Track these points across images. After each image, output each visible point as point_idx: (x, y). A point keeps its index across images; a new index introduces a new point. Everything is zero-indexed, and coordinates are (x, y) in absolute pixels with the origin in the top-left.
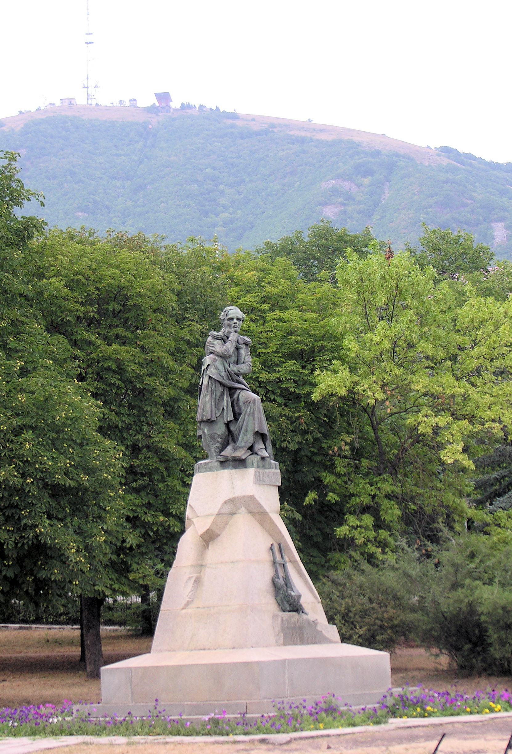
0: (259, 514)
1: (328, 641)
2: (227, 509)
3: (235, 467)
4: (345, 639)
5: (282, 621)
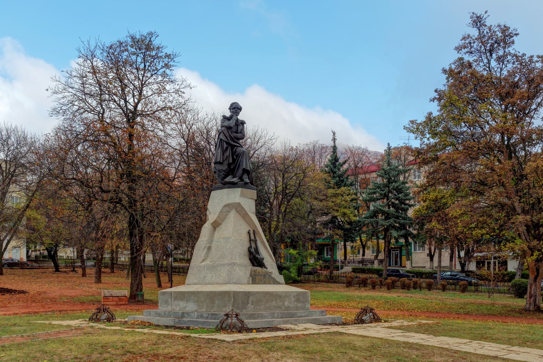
1: (279, 283)
4: (287, 283)
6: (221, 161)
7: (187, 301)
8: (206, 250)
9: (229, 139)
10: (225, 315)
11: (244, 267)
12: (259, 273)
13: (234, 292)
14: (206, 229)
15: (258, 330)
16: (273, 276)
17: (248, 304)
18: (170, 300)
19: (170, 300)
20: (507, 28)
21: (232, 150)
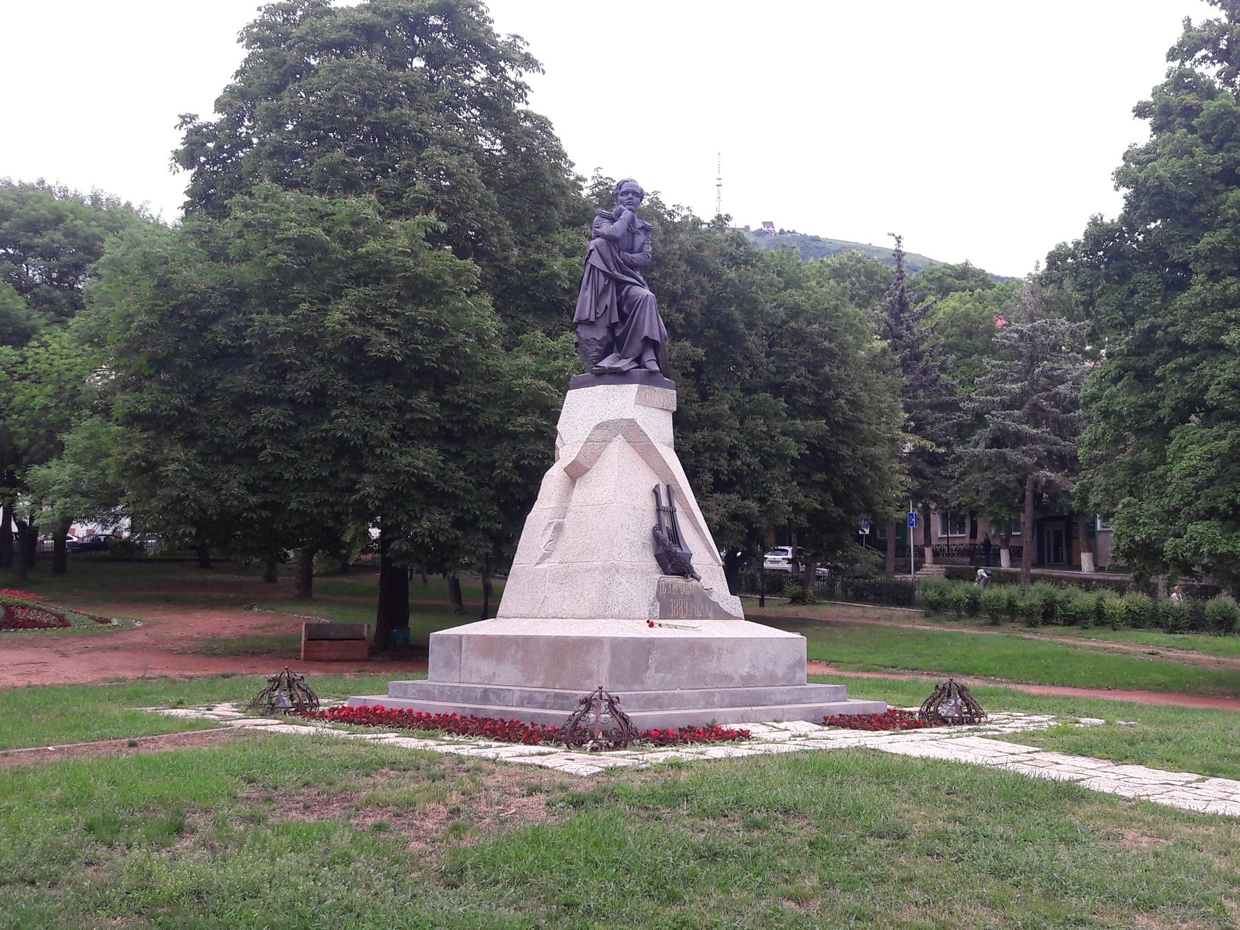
0: (644, 449)
1: (728, 616)
2: (599, 435)
4: (748, 618)
6: (592, 319)
7: (499, 660)
9: (612, 267)
10: (582, 703)
11: (644, 572)
12: (679, 591)
13: (613, 640)
14: (553, 479)
15: (662, 738)
16: (714, 598)
17: (647, 668)
18: (456, 658)
19: (456, 658)
20: (1173, 49)
21: (618, 293)
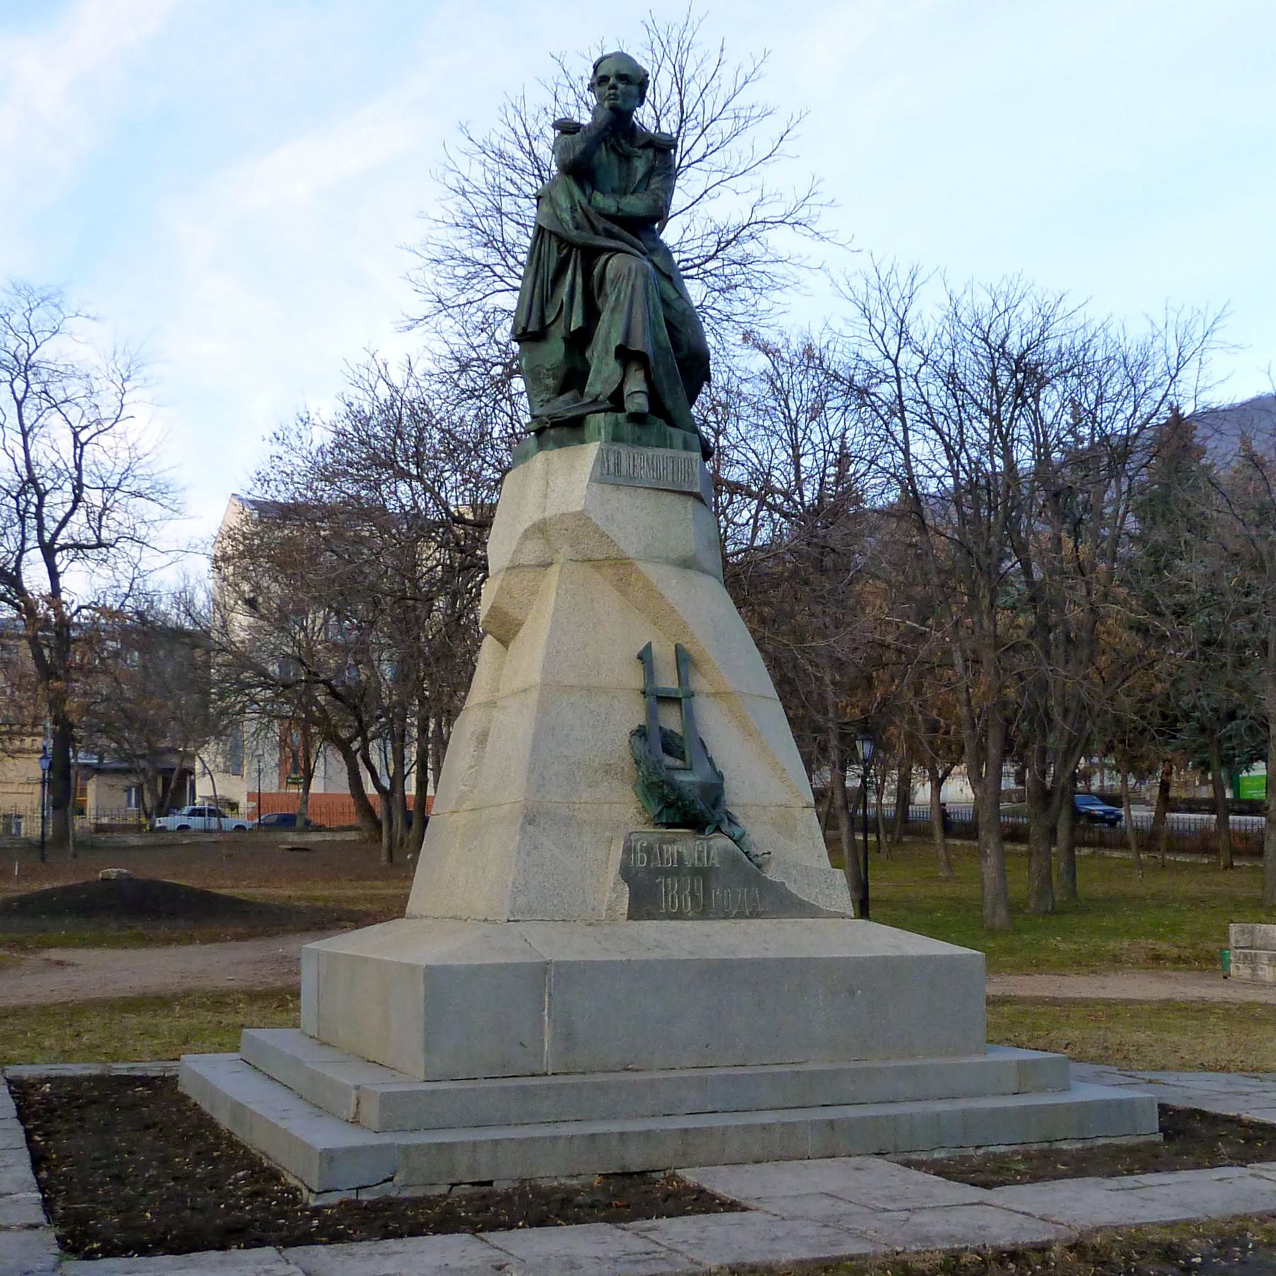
1: (809, 910)
3: (560, 444)
5: (628, 850)
8: (473, 743)
